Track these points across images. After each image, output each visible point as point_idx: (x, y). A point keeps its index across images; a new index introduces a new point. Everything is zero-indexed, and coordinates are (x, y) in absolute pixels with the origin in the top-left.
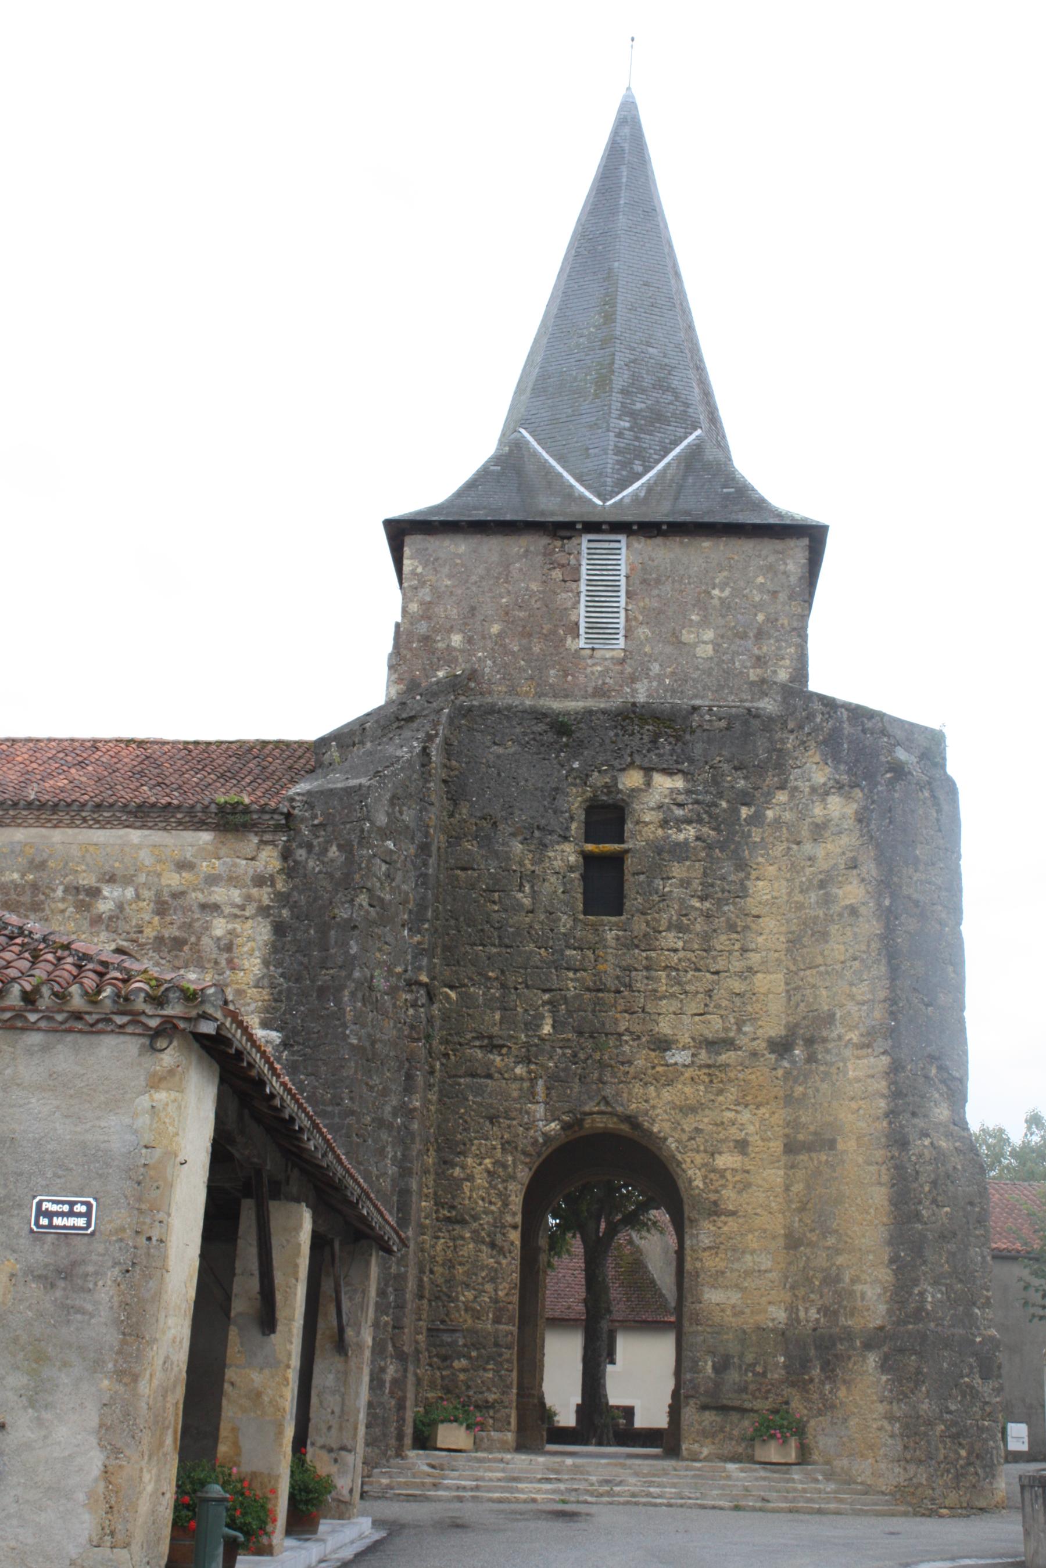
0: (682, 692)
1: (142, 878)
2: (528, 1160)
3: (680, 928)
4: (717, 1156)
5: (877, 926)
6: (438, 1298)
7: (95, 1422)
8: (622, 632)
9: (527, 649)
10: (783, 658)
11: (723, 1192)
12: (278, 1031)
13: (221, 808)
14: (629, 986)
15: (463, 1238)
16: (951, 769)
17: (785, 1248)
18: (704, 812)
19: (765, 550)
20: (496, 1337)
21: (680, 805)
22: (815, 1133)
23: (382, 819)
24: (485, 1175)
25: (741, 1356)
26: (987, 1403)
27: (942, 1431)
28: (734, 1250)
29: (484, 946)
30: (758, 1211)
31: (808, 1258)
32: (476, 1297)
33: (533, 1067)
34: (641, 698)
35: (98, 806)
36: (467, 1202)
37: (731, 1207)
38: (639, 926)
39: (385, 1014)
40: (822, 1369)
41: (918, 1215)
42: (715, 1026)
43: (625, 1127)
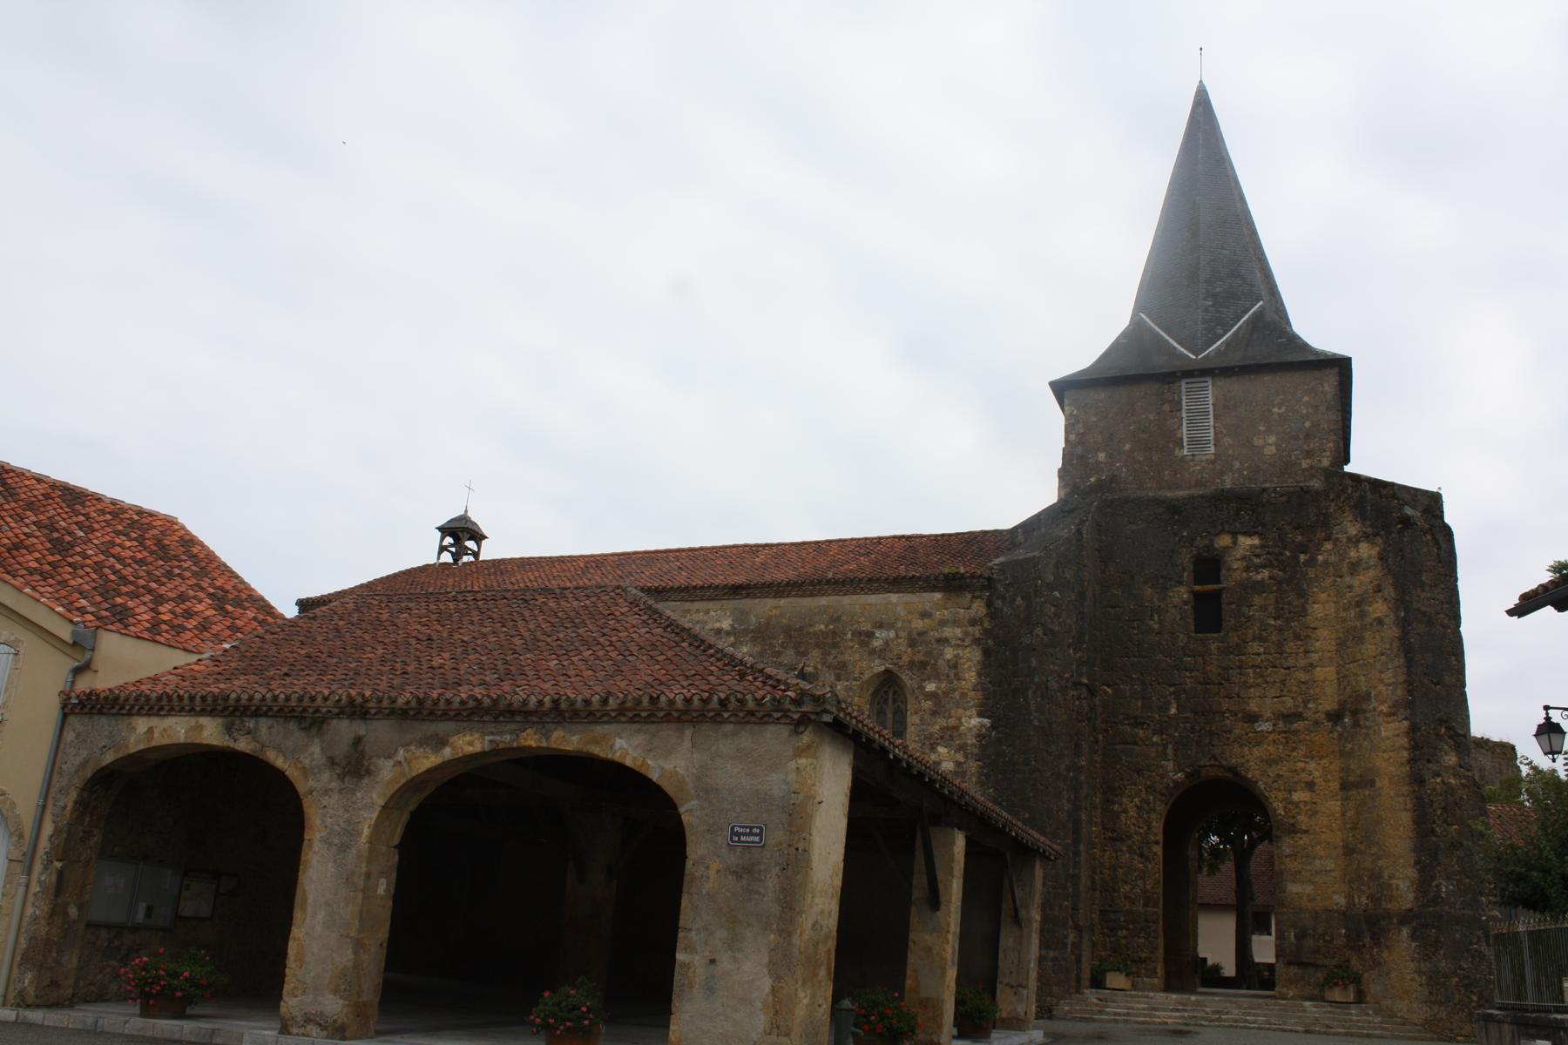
1: (899, 624)
3: (1261, 639)
7: (766, 960)
13: (946, 576)
14: (1228, 680)
21: (1258, 556)
23: (1050, 578)
34: (1228, 485)
35: (870, 580)
38: (1233, 639)
41: (1433, 831)
43: (1229, 775)
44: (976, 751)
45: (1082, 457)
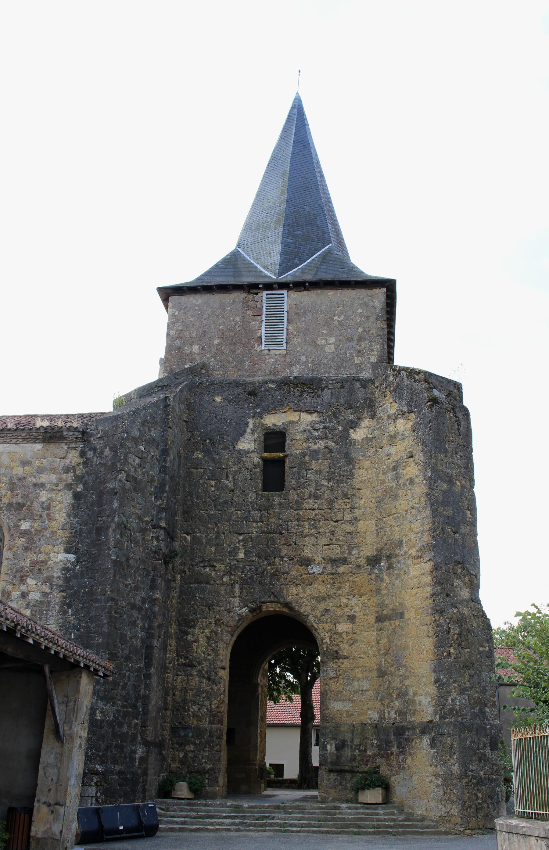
0: (318, 371)
2: (230, 630)
3: (316, 497)
4: (337, 625)
5: (424, 488)
6: (178, 710)
8: (285, 341)
9: (234, 352)
10: (373, 351)
11: (341, 646)
12: (74, 554)
15: (192, 675)
16: (466, 403)
17: (377, 677)
18: (328, 433)
19: (363, 293)
20: (210, 732)
22: (393, 610)
24: (205, 639)
25: (352, 741)
26: (493, 764)
27: (466, 782)
28: (348, 679)
29: (206, 510)
30: (362, 656)
31: (390, 682)
32: (199, 709)
33: (233, 577)
36: (195, 654)
37: (345, 654)
39: (137, 544)
40: (398, 747)
42: (336, 551)
43: (285, 610)
44: (60, 583)
45: (179, 349)
